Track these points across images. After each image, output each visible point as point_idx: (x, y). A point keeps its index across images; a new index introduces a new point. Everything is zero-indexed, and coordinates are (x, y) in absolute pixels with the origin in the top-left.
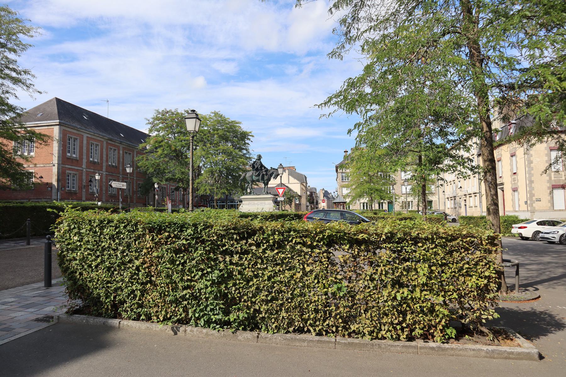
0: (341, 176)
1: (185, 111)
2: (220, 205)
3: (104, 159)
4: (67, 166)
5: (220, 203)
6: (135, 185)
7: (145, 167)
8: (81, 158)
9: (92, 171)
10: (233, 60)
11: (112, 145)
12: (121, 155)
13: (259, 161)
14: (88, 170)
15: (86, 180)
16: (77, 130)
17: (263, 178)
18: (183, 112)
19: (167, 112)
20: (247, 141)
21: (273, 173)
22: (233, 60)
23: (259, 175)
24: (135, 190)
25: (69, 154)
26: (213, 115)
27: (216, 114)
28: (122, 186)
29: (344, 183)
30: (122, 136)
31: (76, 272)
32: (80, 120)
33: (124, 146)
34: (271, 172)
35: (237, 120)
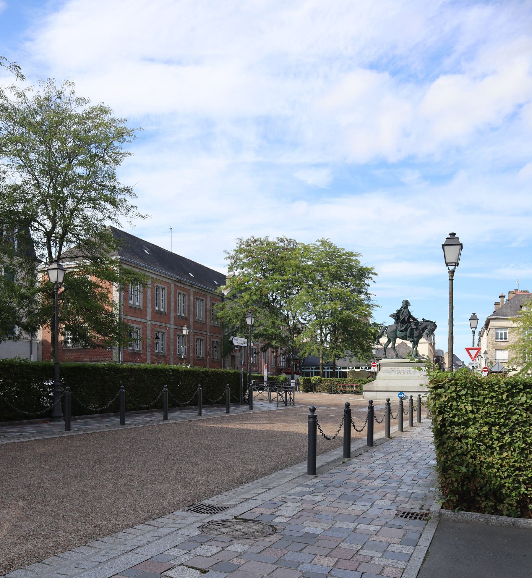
0: (494, 333)
1: (279, 240)
2: (328, 372)
3: (172, 308)
4: (129, 318)
5: (328, 369)
6: (208, 343)
7: (226, 318)
8: (145, 307)
9: (158, 323)
10: (325, 165)
11: (180, 288)
12: (192, 302)
13: (406, 310)
14: (154, 323)
15: (151, 337)
16: (140, 269)
17: (411, 335)
18: (276, 241)
19: (255, 242)
20: (366, 282)
21: (425, 328)
22: (325, 165)
23: (406, 330)
24: (208, 350)
25: (131, 302)
26: (319, 244)
27: (323, 242)
28: (243, 342)
29: (499, 343)
30: (192, 276)
31: (466, 455)
32: (142, 256)
33: (195, 290)
34: (423, 325)
35: (355, 250)
